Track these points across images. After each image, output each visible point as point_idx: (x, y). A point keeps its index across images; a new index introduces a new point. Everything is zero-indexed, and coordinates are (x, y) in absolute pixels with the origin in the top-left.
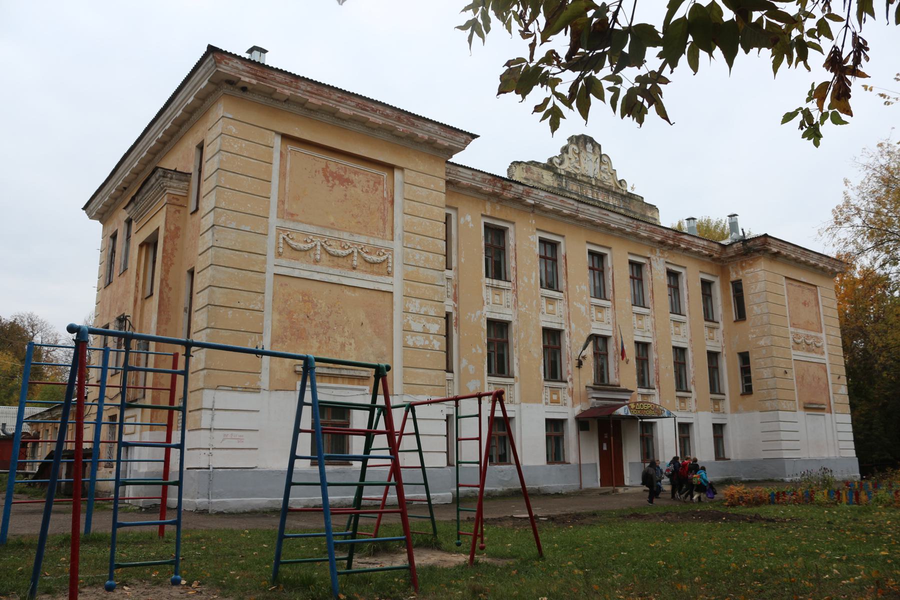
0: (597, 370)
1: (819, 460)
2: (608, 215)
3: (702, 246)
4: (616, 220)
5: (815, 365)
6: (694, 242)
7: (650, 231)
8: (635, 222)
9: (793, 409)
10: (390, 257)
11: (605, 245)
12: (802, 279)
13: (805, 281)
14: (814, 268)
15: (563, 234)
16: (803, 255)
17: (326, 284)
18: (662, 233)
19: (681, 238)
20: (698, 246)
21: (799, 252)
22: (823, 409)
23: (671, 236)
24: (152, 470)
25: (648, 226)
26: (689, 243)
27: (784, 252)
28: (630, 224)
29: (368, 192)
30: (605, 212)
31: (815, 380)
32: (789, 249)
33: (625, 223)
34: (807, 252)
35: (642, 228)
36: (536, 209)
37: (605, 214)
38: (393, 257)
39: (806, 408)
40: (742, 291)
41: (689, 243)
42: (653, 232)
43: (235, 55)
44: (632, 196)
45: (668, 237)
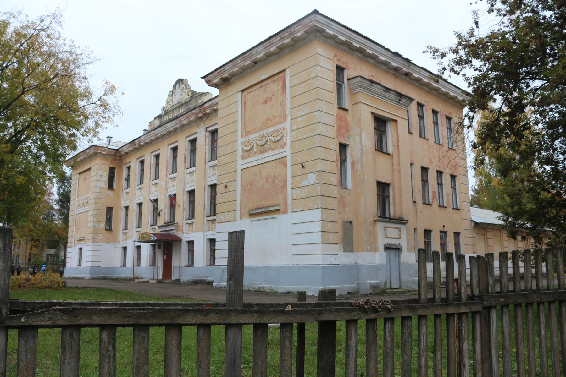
1: (254, 268)
5: (272, 164)
7: (187, 118)
8: (178, 119)
9: (231, 219)
10: (285, 133)
12: (263, 77)
13: (267, 76)
14: (269, 58)
15: (176, 140)
16: (245, 60)
18: (193, 114)
21: (239, 61)
22: (277, 211)
24: (328, 262)
25: (184, 116)
26: (210, 106)
27: (226, 75)
31: (269, 180)
32: (228, 68)
34: (247, 55)
35: (182, 120)
36: (147, 144)
37: (165, 127)
39: (251, 215)
40: (110, 173)
41: (210, 107)
45: (197, 114)
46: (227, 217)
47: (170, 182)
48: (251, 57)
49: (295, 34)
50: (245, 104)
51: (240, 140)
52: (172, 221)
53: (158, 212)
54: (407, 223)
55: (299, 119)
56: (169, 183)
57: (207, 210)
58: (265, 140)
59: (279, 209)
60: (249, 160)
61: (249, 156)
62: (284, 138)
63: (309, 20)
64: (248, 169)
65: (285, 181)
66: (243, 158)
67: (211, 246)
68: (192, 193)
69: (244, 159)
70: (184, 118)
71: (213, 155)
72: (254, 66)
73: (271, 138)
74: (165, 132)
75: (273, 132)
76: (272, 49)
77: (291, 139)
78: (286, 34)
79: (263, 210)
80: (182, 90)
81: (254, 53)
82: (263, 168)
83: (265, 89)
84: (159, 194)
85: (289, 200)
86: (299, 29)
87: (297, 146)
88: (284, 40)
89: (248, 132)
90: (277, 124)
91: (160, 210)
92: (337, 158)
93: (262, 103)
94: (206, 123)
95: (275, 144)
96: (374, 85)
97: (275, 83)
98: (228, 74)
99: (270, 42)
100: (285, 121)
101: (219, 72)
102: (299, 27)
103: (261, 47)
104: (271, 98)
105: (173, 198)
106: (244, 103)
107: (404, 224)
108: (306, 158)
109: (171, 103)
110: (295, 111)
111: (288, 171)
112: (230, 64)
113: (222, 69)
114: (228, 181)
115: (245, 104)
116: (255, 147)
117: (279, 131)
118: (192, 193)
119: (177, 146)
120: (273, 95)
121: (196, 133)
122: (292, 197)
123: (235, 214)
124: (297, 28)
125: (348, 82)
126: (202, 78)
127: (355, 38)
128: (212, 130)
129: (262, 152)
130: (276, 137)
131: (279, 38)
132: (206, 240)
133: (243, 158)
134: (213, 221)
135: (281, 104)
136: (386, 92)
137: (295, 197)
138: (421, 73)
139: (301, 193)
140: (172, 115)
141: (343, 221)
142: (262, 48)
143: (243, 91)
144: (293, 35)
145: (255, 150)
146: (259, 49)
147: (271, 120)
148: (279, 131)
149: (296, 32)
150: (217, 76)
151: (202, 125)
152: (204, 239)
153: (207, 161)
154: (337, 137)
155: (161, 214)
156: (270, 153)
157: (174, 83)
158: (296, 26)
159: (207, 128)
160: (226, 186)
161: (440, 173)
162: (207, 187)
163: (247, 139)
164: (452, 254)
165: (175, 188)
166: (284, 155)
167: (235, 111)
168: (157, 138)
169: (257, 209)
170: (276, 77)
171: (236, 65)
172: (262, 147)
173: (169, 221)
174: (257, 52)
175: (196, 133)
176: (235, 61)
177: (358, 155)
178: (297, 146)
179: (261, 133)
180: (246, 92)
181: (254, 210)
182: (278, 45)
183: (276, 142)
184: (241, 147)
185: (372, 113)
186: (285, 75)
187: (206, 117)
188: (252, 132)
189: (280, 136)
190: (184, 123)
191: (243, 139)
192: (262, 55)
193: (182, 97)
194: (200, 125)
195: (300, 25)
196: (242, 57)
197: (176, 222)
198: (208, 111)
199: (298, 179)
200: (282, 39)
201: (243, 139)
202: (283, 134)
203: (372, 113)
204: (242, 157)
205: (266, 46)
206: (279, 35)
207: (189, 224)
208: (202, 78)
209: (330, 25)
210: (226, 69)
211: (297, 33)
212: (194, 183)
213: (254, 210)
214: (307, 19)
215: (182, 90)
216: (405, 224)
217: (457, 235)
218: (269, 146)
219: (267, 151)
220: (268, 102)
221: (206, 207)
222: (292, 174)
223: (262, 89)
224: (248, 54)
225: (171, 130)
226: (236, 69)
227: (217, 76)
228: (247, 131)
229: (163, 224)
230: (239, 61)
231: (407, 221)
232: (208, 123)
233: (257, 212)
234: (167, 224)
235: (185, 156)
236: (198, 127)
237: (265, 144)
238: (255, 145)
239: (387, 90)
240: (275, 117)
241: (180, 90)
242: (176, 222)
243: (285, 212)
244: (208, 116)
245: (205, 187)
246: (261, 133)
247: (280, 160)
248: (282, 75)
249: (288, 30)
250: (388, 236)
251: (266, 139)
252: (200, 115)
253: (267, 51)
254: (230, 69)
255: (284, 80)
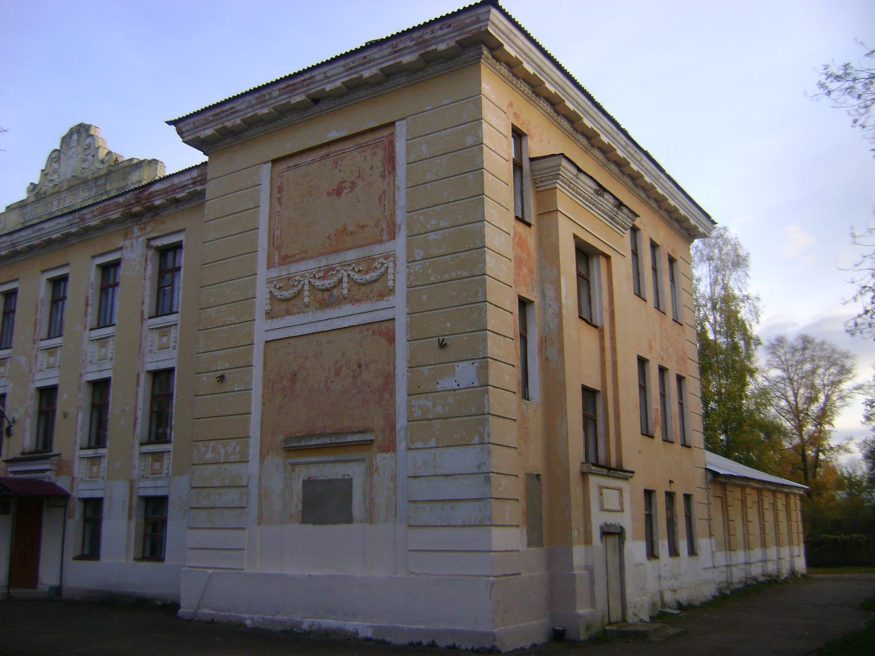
0: (167, 420)
2: (43, 229)
3: (190, 182)
4: (54, 229)
6: (173, 185)
7: (100, 214)
8: (77, 215)
10: (391, 265)
11: (105, 250)
12: (334, 135)
13: (343, 134)
17: (338, 331)
18: (118, 206)
19: (150, 194)
20: (184, 187)
21: (275, 94)
23: (133, 201)
25: (94, 208)
26: (165, 191)
28: (72, 222)
29: (384, 179)
30: (38, 227)
33: (65, 225)
34: (296, 81)
35: (87, 217)
37: (39, 230)
38: (395, 267)
41: (166, 193)
42: (105, 212)
43: (476, 4)
44: (25, 203)
45: (129, 205)
46: (223, 452)
47: (43, 358)
48: (308, 85)
49: (432, 45)
50: (280, 192)
51: (263, 273)
52: (40, 448)
53: (6, 425)
54: (631, 477)
55: (432, 236)
56: (39, 359)
57: (142, 429)
58: (336, 279)
59: (372, 441)
60: (289, 320)
61: (289, 313)
62: (390, 277)
63: (474, 18)
64: (286, 342)
65: (389, 378)
66: (270, 315)
67: (146, 512)
68: (101, 387)
69: (272, 318)
70: (92, 212)
71: (103, 304)
72: (310, 108)
73: (352, 273)
74: (38, 241)
75: (358, 261)
76: (366, 74)
77: (408, 279)
78: (409, 44)
79: (327, 440)
80: (85, 149)
81: (317, 78)
82: (328, 342)
83: (336, 163)
84: (11, 385)
85: (401, 422)
86: (444, 35)
87: (424, 297)
88: (402, 56)
89: (287, 256)
90: (370, 244)
91: (11, 420)
92: (515, 333)
93: (329, 194)
94: (149, 229)
95: (363, 289)
96: (582, 177)
97: (365, 151)
98: (242, 120)
99: (365, 58)
100: (393, 236)
101: (218, 114)
102: (446, 31)
103: (339, 67)
104: (353, 183)
105: (48, 394)
106: (278, 191)
107: (626, 479)
108: (448, 325)
109: (55, 177)
110: (421, 218)
111: (397, 353)
112: (248, 98)
113: (227, 107)
114: (227, 365)
115: (280, 192)
116: (306, 293)
117: (374, 259)
118: (101, 387)
119: (68, 274)
120: (359, 177)
121: (121, 249)
122: (410, 413)
123: (246, 445)
124: (440, 33)
125: (531, 165)
126: (170, 123)
127: (550, 73)
128: (164, 246)
129: (324, 305)
130: (367, 273)
131: (390, 50)
132: (135, 498)
133: (270, 315)
134: (158, 456)
135: (380, 200)
136: (597, 194)
137: (418, 414)
138: (643, 162)
139: (434, 405)
140: (55, 203)
141: (526, 474)
142: (342, 69)
143: (275, 162)
144: (428, 46)
145: (306, 300)
146: (331, 70)
147: (352, 233)
148: (374, 259)
149: (436, 40)
150: (211, 121)
151: (136, 231)
152: (131, 497)
153: (146, 316)
154: (515, 283)
155: (15, 429)
156: (348, 308)
157: (65, 132)
158: (437, 27)
159: (149, 240)
160: (222, 378)
161: (662, 370)
162: (143, 376)
163: (284, 273)
164: (307, 483)
165: (56, 372)
166: (388, 315)
167: (252, 205)
168: (15, 254)
169: (310, 436)
170: (369, 138)
171: (265, 101)
172: (326, 295)
173: (33, 448)
174: (327, 77)
175: (121, 249)
176: (264, 92)
177: (552, 325)
178: (424, 297)
179: (323, 262)
180: (282, 166)
181: (302, 438)
182: (383, 66)
183: (365, 285)
184: (268, 291)
185: (575, 237)
186: (392, 134)
187: (151, 214)
188: (297, 257)
189: (378, 272)
190: (92, 224)
191: (274, 273)
192: (338, 84)
193: (85, 165)
194: (132, 232)
195: (449, 26)
196: (283, 85)
197: (55, 452)
198: (158, 202)
199: (426, 373)
200: (396, 52)
201: (274, 273)
202: (387, 268)
203: (575, 237)
204: (267, 313)
205: (352, 65)
206: (389, 44)
207: (89, 458)
208: (170, 123)
209: (512, 36)
210: (238, 108)
211: (437, 43)
212: (108, 365)
213: (302, 438)
214: (468, 14)
215: (85, 149)
216: (627, 479)
217: (687, 497)
218: (345, 292)
219: (339, 304)
220: (345, 191)
221: (139, 421)
222: (409, 361)
223: (329, 162)
224: (303, 78)
225: (54, 237)
226: (265, 111)
227: (211, 121)
228: (283, 253)
229: (19, 456)
230: (275, 94)
231: (633, 472)
232: (152, 230)
233: (308, 443)
234: (27, 457)
235: (87, 301)
236: (126, 236)
237: (334, 287)
238: (306, 287)
239: (601, 190)
240: (363, 227)
241: (80, 150)
242: (55, 452)
243: (390, 447)
244: (157, 214)
245: (138, 374)
246: (323, 262)
247: (376, 327)
248: (385, 133)
249: (415, 35)
250: (606, 507)
251: (340, 276)
252: (136, 209)
253: (353, 76)
254: (247, 107)
255: (392, 144)
